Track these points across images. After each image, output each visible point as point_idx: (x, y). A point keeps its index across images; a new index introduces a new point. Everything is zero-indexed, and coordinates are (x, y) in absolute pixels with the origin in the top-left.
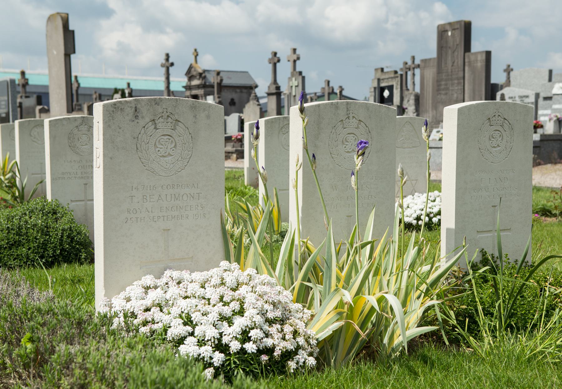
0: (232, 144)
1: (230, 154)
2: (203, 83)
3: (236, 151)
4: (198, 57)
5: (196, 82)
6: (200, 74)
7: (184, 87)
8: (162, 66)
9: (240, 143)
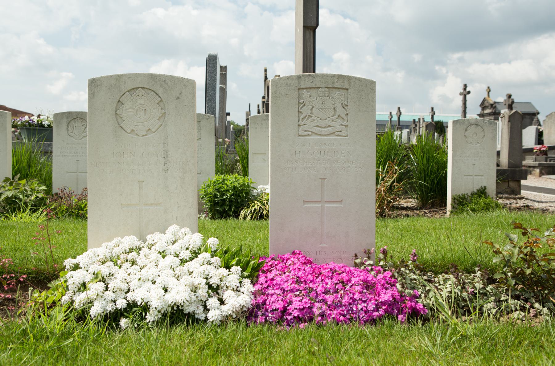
0: (534, 157)
1: (531, 169)
2: (494, 111)
3: (540, 165)
4: (490, 93)
5: (488, 111)
6: (492, 105)
7: (478, 115)
8: (461, 94)
9: (544, 156)
